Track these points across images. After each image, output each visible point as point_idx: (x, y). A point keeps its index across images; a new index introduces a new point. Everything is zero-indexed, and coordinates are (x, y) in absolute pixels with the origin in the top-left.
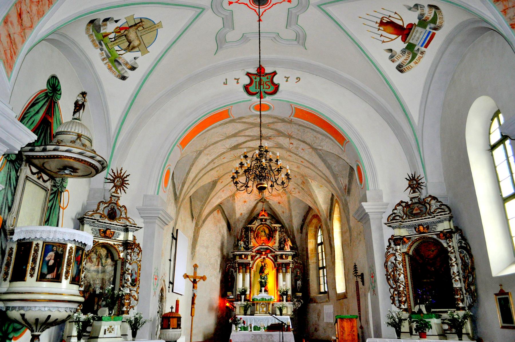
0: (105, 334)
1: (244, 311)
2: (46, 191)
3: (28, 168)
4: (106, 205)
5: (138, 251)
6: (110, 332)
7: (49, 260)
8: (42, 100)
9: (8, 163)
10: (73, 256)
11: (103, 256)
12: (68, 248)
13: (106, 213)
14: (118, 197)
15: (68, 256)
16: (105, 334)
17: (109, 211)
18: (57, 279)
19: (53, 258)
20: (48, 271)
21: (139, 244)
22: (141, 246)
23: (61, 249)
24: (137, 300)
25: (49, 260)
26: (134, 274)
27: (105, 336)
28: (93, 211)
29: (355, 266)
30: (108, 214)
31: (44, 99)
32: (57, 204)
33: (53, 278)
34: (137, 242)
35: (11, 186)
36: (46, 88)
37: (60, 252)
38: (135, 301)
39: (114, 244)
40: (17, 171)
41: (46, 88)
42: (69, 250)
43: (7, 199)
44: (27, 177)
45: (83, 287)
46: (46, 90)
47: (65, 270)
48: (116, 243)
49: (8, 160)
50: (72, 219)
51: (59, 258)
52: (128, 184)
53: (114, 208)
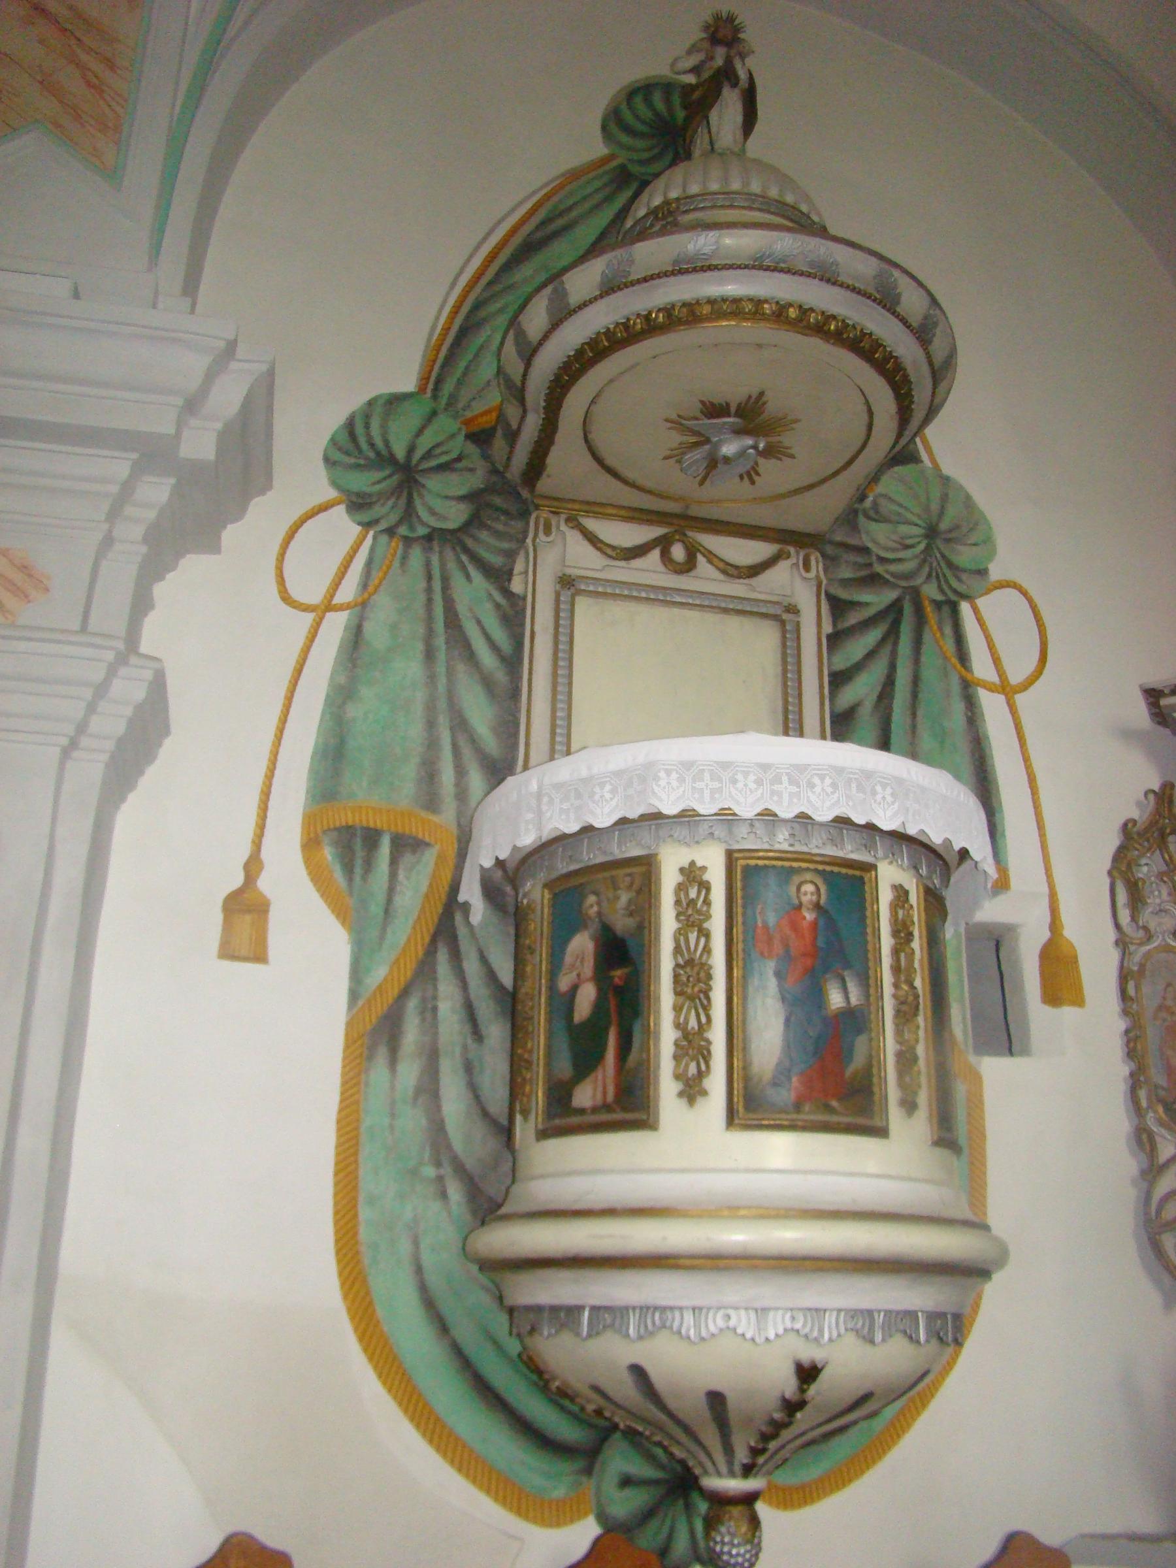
2: (775, 617)
3: (574, 539)
4: (362, 462)
7: (574, 988)
8: (598, 206)
9: (416, 554)
10: (916, 944)
12: (669, 880)
15: (680, 934)
18: (631, 1108)
19: (588, 969)
20: (576, 1066)
23: (624, 898)
25: (574, 988)
31: (608, 199)
32: (929, 674)
33: (606, 1107)
35: (470, 656)
36: (600, 149)
37: (622, 923)
40: (500, 576)
41: (600, 149)
42: (680, 888)
43: (460, 724)
44: (567, 582)
46: (612, 157)
47: (667, 1037)
49: (408, 541)
50: (1128, 735)
51: (622, 957)
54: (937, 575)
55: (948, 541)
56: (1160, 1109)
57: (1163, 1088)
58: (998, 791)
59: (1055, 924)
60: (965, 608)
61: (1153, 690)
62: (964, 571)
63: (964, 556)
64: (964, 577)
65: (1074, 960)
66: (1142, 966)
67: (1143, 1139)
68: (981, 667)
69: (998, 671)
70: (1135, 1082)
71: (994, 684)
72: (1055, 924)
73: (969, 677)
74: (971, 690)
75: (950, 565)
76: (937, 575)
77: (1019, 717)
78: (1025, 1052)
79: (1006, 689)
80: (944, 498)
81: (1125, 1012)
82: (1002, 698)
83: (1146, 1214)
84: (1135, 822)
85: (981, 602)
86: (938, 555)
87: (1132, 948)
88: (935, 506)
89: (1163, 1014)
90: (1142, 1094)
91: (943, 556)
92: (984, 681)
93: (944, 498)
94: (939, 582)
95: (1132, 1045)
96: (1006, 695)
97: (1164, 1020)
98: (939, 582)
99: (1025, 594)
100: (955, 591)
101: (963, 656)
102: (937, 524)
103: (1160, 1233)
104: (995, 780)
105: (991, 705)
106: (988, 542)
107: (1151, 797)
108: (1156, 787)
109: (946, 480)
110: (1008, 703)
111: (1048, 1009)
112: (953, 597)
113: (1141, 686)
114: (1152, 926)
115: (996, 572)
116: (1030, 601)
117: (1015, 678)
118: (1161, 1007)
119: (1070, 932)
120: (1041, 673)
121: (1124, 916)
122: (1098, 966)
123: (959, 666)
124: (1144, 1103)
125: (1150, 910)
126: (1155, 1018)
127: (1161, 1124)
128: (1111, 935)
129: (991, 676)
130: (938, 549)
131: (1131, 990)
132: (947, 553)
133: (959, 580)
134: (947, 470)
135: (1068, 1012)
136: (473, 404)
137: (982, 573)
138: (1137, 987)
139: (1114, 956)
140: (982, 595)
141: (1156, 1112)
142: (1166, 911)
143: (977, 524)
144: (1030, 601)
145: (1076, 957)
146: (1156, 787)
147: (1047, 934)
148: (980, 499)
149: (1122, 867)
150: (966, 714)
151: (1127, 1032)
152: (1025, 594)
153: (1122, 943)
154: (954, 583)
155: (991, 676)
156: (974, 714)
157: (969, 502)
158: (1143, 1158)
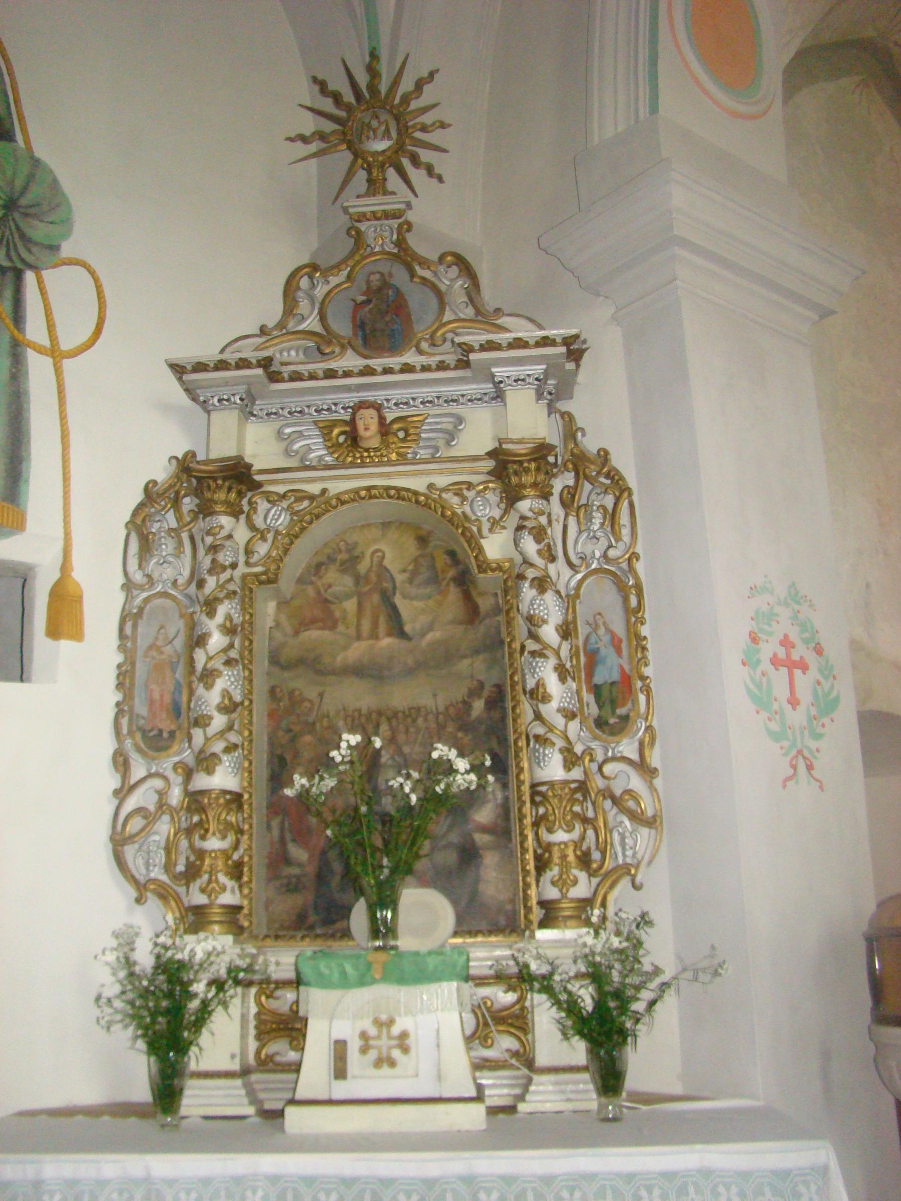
0: (340, 1072)
1: (368, 408)
5: (609, 501)
6: (385, 1061)
11: (400, 578)
13: (342, 327)
14: (396, 215)
16: (340, 1072)
17: (358, 306)
21: (604, 456)
22: (624, 462)
24: (651, 822)
26: (606, 651)
27: (341, 1090)
28: (263, 331)
29: (301, 105)
30: (360, 326)
34: (591, 444)
38: (645, 831)
39: (431, 486)
45: (294, 791)
48: (442, 481)
52: (322, 86)
53: (385, 284)
54: (8, 244)
55: (26, 215)
56: (138, 736)
57: (143, 718)
58: (29, 441)
59: (66, 566)
60: (30, 277)
61: (177, 365)
62: (36, 244)
63: (38, 231)
64: (35, 249)
65: (79, 599)
66: (141, 610)
67: (121, 762)
68: (35, 329)
69: (50, 336)
70: (120, 709)
71: (44, 347)
72: (66, 566)
73: (21, 337)
74: (19, 349)
75: (23, 236)
76: (8, 244)
77: (63, 379)
78: (29, 680)
79: (55, 353)
80: (31, 177)
81: (122, 648)
82: (50, 360)
83: (114, 827)
84: (155, 483)
85: (45, 274)
86: (13, 227)
87: (135, 592)
88: (19, 184)
89: (154, 653)
90: (125, 722)
91: (18, 229)
92: (35, 343)
93: (31, 177)
94: (8, 250)
95: (121, 678)
96: (54, 358)
97: (154, 658)
98: (8, 250)
99: (92, 273)
100: (23, 261)
101: (18, 317)
102: (18, 199)
103: (123, 845)
104: (28, 430)
105: (38, 367)
106: (67, 224)
107: (174, 462)
108: (180, 456)
109: (36, 163)
110: (55, 365)
111: (49, 641)
112: (19, 265)
113: (166, 361)
114: (155, 576)
115: (67, 250)
116: (96, 280)
117: (66, 343)
118: (151, 647)
119: (79, 574)
120: (93, 344)
121: (133, 564)
122: (102, 607)
123: (12, 327)
124: (125, 731)
125: (155, 560)
126: (145, 656)
127: (139, 750)
128: (121, 580)
129: (44, 340)
130: (14, 220)
131: (128, 630)
132: (21, 224)
133: (30, 252)
134: (39, 153)
135: (65, 645)
136: (331, 87)
137: (54, 248)
138: (135, 626)
139: (121, 597)
140: (47, 269)
141: (134, 738)
142: (170, 563)
143: (58, 206)
144: (96, 280)
145: (81, 597)
146: (180, 456)
147: (57, 575)
148: (67, 185)
149: (140, 526)
150: (11, 371)
151: (119, 666)
152: (92, 273)
153: (128, 586)
154: (24, 254)
155: (44, 340)
156: (19, 370)
157: (55, 185)
158: (118, 777)
